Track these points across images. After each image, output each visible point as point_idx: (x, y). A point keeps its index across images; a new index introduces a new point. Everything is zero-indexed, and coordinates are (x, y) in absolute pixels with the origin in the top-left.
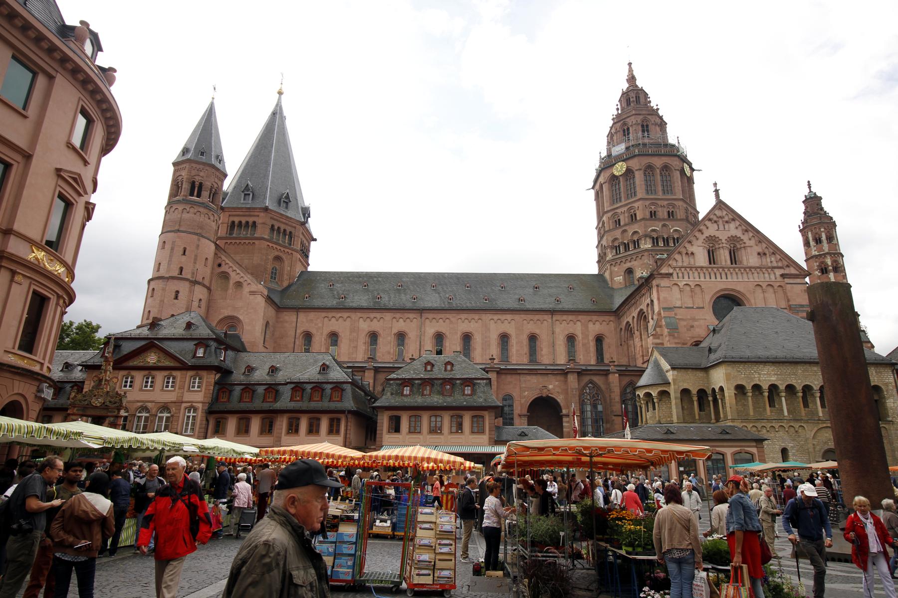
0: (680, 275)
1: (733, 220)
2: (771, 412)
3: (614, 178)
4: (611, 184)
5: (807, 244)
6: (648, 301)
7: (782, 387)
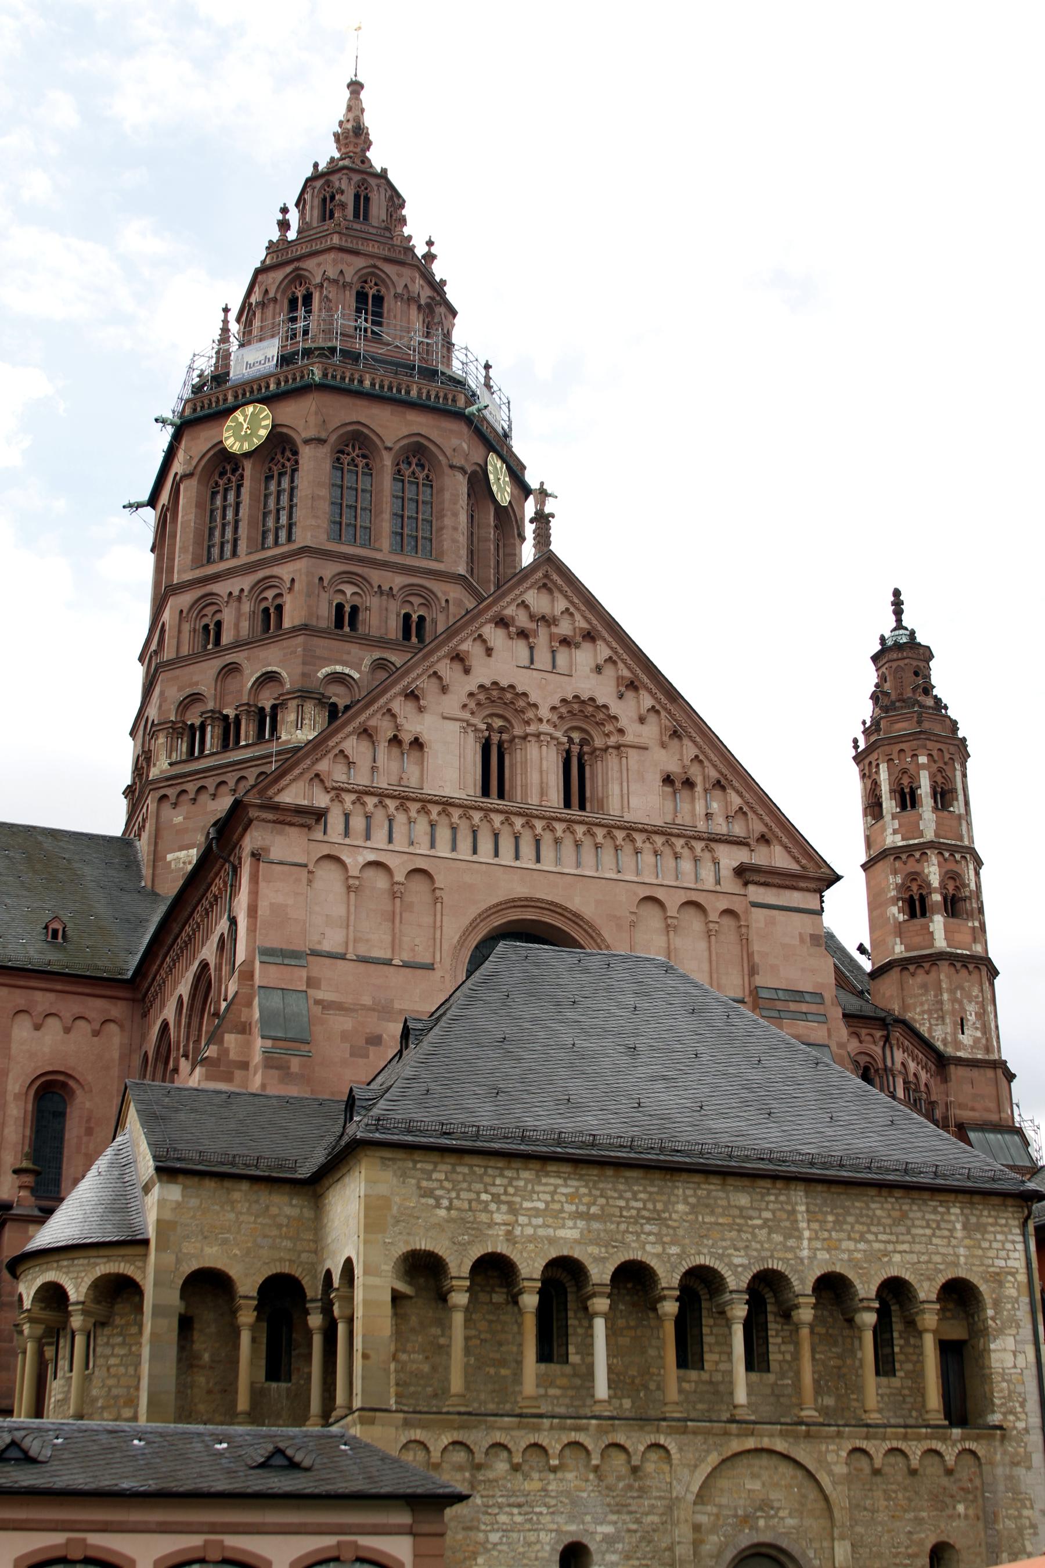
0: (358, 823)
1: (590, 636)
2: (542, 1381)
3: (224, 462)
4: (213, 480)
5: (873, 807)
6: (223, 926)
7: (600, 1273)
